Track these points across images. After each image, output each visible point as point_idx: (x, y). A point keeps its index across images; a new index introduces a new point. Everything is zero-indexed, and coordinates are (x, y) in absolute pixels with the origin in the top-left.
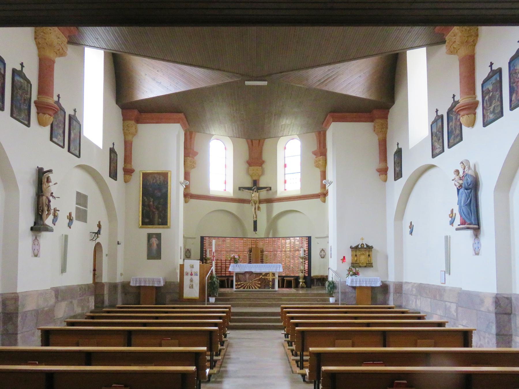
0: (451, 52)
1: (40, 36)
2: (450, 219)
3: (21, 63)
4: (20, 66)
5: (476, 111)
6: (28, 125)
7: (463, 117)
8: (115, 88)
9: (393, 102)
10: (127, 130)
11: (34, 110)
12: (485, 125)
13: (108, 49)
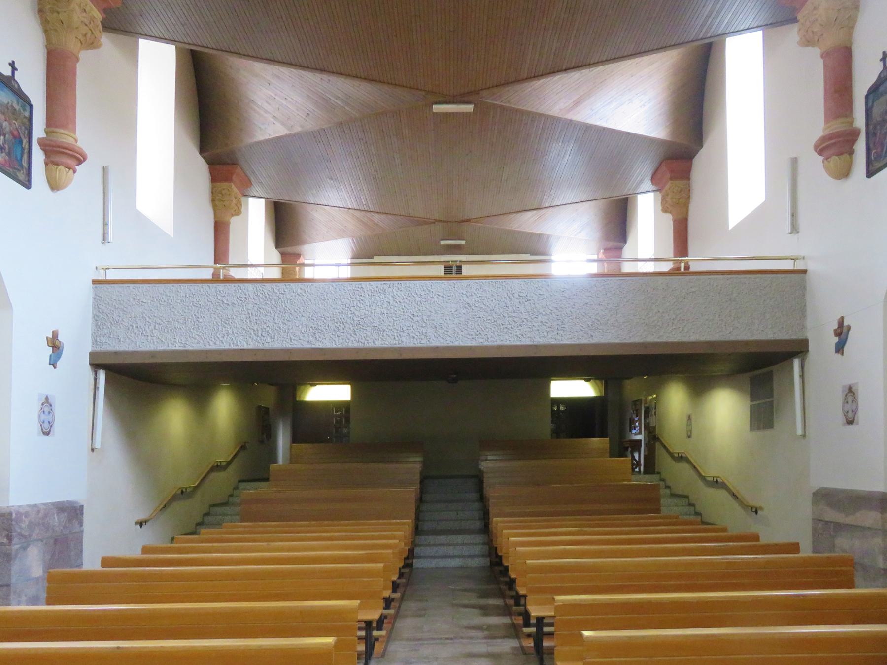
0: (808, 42)
1: (218, 197)
2: (836, 339)
3: (11, 62)
4: (10, 68)
5: (854, 148)
6: (27, 184)
7: (829, 160)
8: (274, 221)
9: (701, 145)
10: (53, 11)
11: (38, 157)
12: (870, 174)
13: (181, 42)
